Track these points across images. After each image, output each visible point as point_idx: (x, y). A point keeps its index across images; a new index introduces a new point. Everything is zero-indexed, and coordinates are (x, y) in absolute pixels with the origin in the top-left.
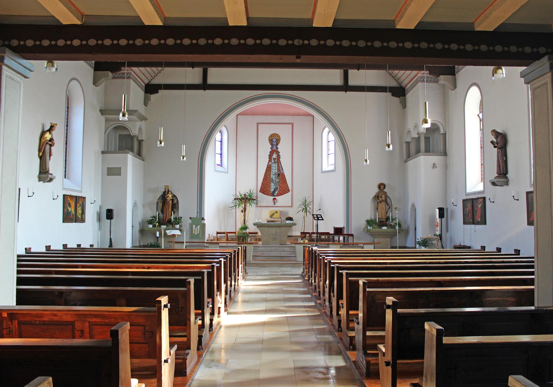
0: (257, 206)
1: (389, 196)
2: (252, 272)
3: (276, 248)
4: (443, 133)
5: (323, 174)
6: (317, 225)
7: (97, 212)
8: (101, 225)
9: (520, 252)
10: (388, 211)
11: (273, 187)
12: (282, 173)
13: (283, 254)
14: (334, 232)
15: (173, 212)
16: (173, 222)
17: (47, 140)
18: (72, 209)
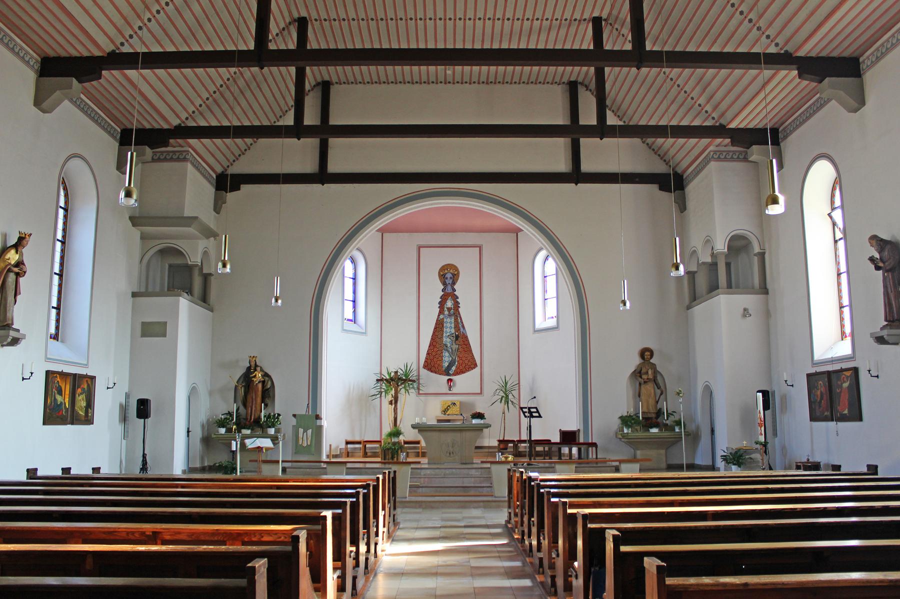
0: (419, 394)
2: (410, 520)
3: (454, 470)
4: (759, 253)
5: (537, 335)
6: (530, 426)
7: (121, 405)
8: (128, 428)
9: (878, 469)
10: (659, 400)
11: (446, 359)
13: (467, 482)
14: (560, 439)
15: (263, 404)
16: (263, 423)
17: (10, 264)
18: (64, 400)
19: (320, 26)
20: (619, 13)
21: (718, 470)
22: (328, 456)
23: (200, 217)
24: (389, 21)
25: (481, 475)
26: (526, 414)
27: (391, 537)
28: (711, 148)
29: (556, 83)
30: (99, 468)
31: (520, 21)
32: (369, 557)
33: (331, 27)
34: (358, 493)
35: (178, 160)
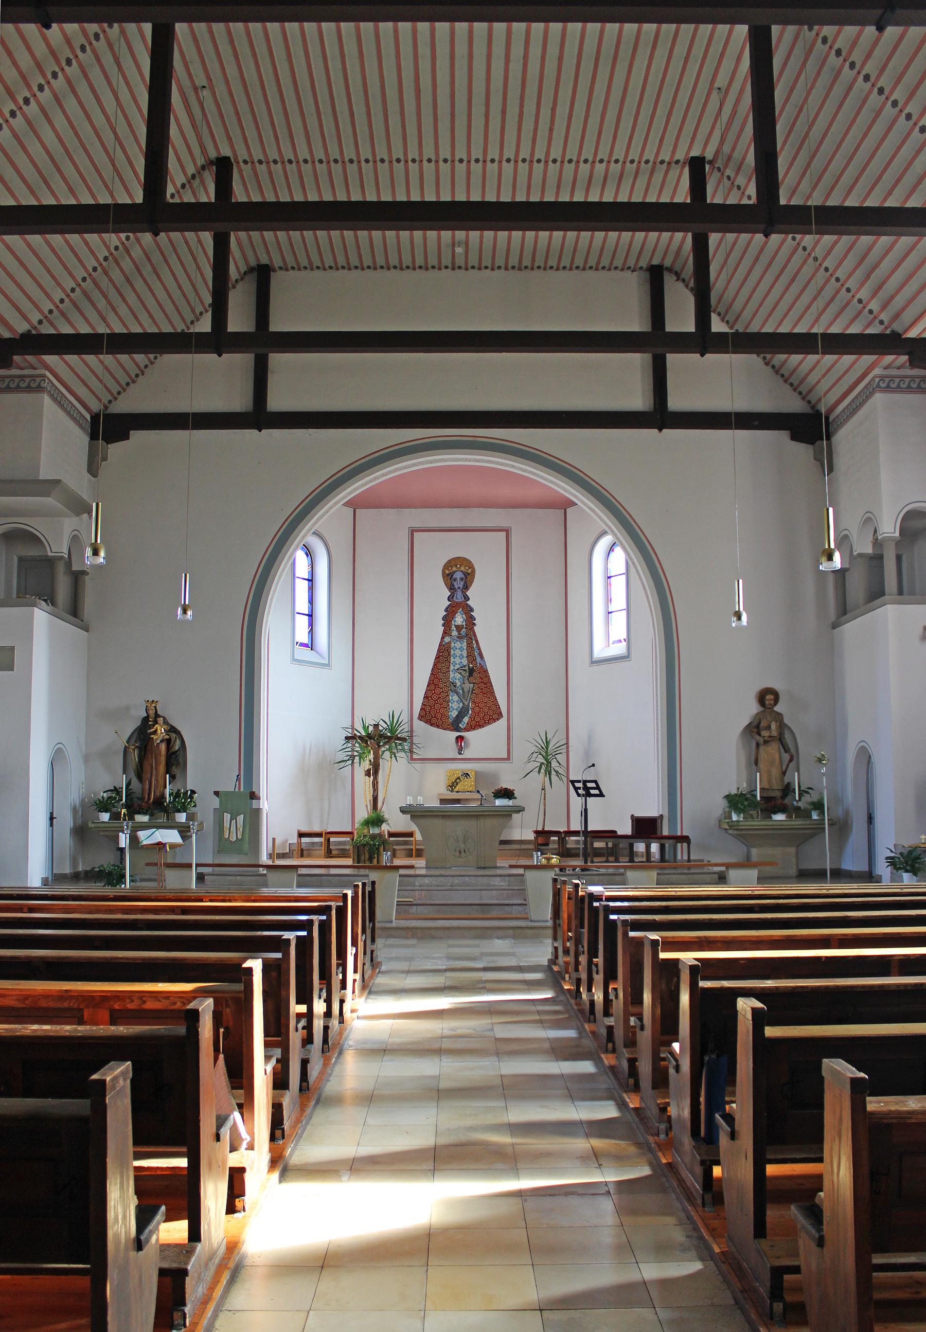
0: (412, 759)
1: (790, 725)
2: (397, 959)
3: (467, 878)
5: (595, 668)
6: (586, 810)
11: (455, 705)
12: (482, 667)
13: (488, 898)
19: (251, 171)
20: (733, 149)
21: (878, 880)
22: (270, 856)
23: (64, 480)
24: (363, 163)
25: (509, 885)
26: (580, 791)
27: (367, 988)
28: (877, 371)
29: (629, 268)
31: (573, 165)
32: (330, 1025)
33: (270, 173)
34: (311, 922)
35: (29, 389)
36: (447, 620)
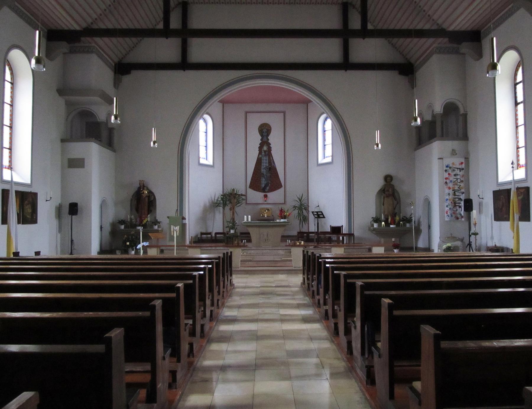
4: (463, 114)
5: (319, 167)
11: (263, 182)
28: (434, 45)
30: (40, 252)
36: (260, 148)
